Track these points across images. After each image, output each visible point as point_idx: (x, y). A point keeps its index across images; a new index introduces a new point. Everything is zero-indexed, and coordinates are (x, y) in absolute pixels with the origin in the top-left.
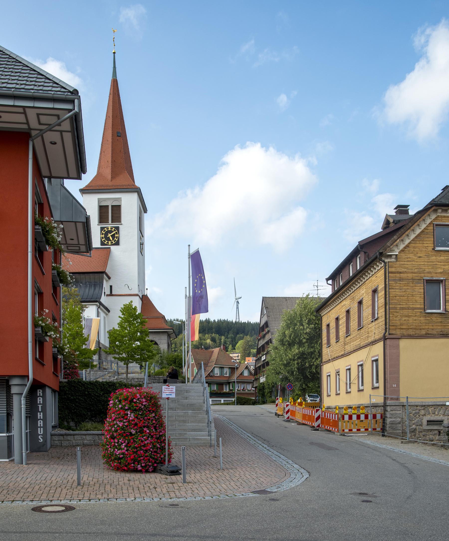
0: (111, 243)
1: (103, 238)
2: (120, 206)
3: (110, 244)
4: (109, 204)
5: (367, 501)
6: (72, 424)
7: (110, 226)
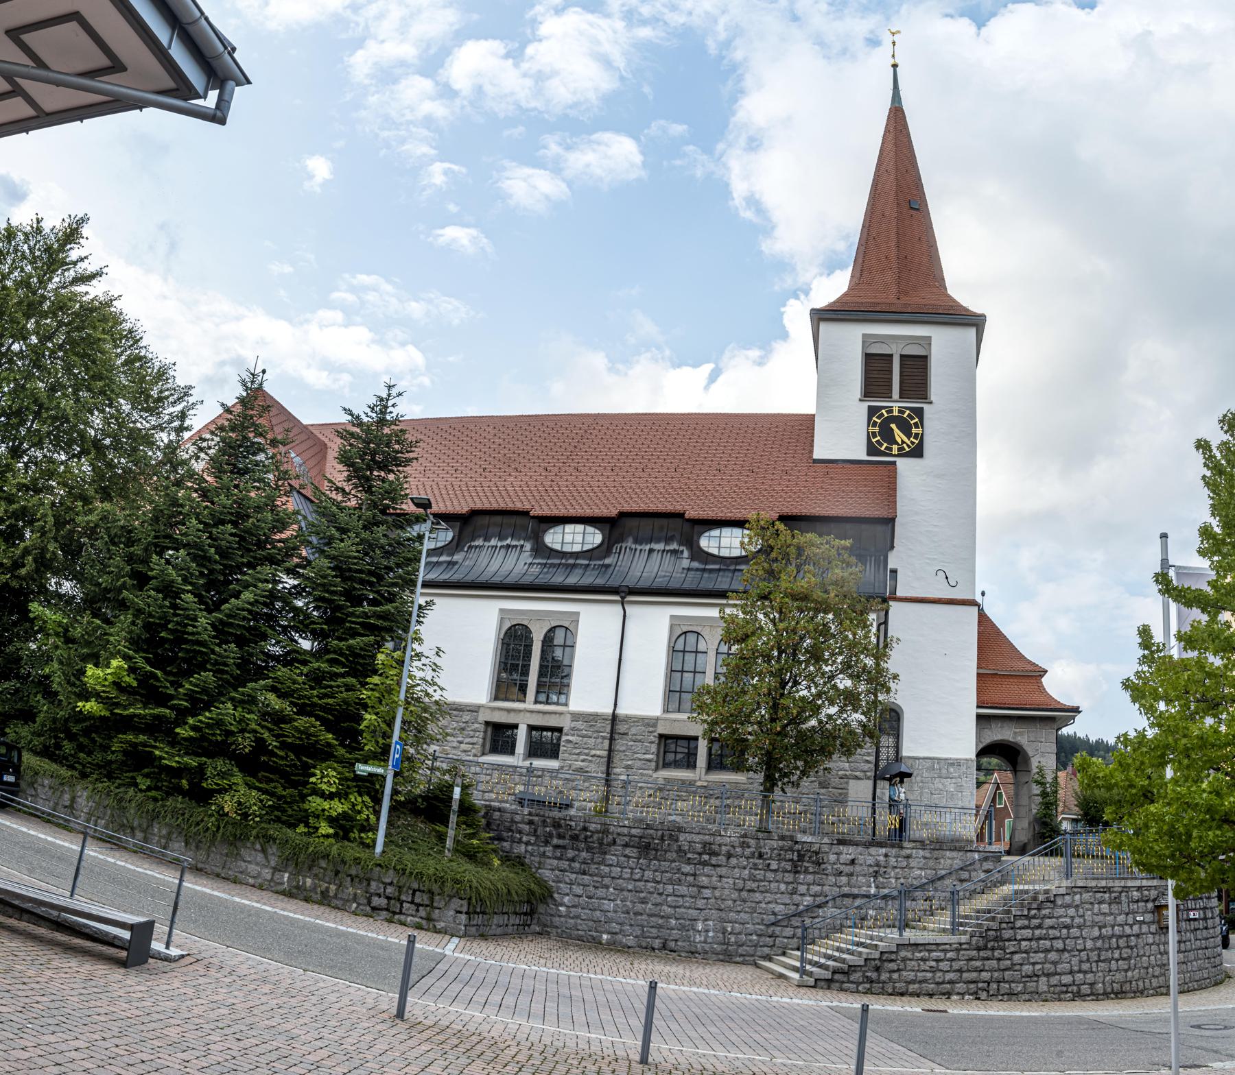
0: (899, 450)
1: (875, 436)
2: (926, 357)
3: (895, 451)
4: (896, 351)
5: (1199, 1027)
6: (554, 698)
7: (896, 407)
